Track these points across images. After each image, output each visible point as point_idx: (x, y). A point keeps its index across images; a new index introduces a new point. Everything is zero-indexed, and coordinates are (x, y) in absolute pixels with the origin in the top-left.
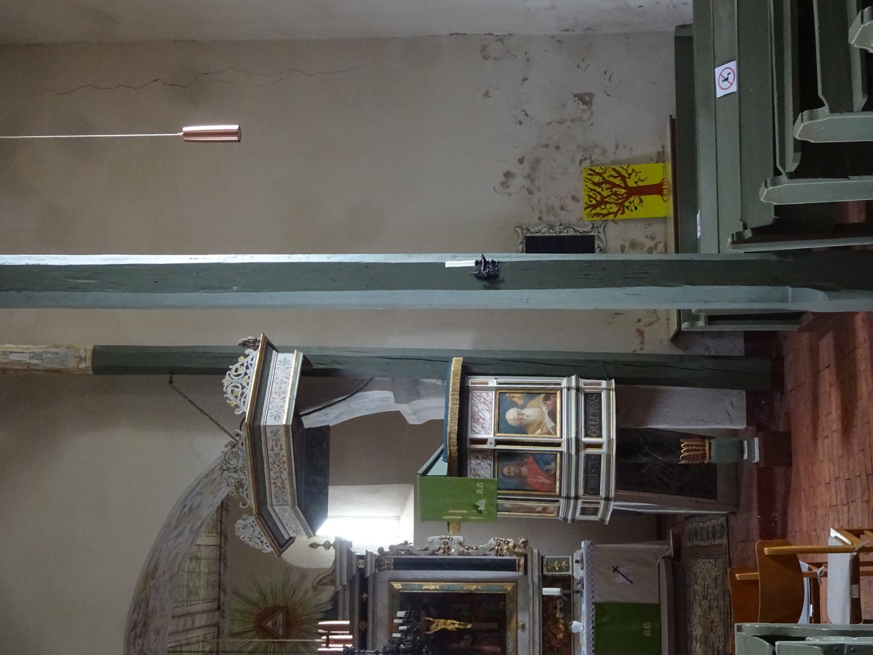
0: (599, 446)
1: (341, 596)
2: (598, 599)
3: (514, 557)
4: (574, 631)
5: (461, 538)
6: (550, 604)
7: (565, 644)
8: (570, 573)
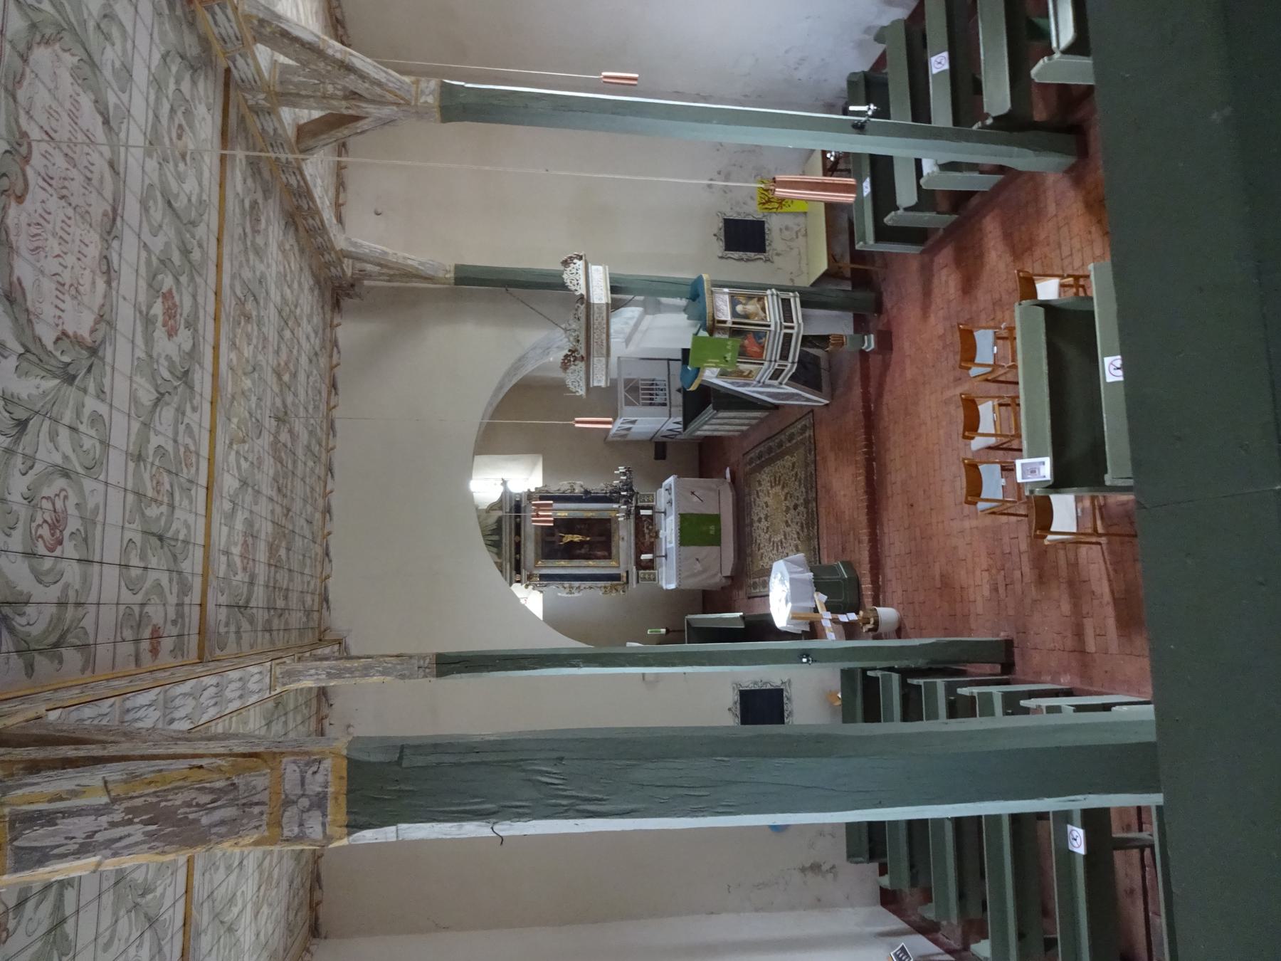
0: (792, 328)
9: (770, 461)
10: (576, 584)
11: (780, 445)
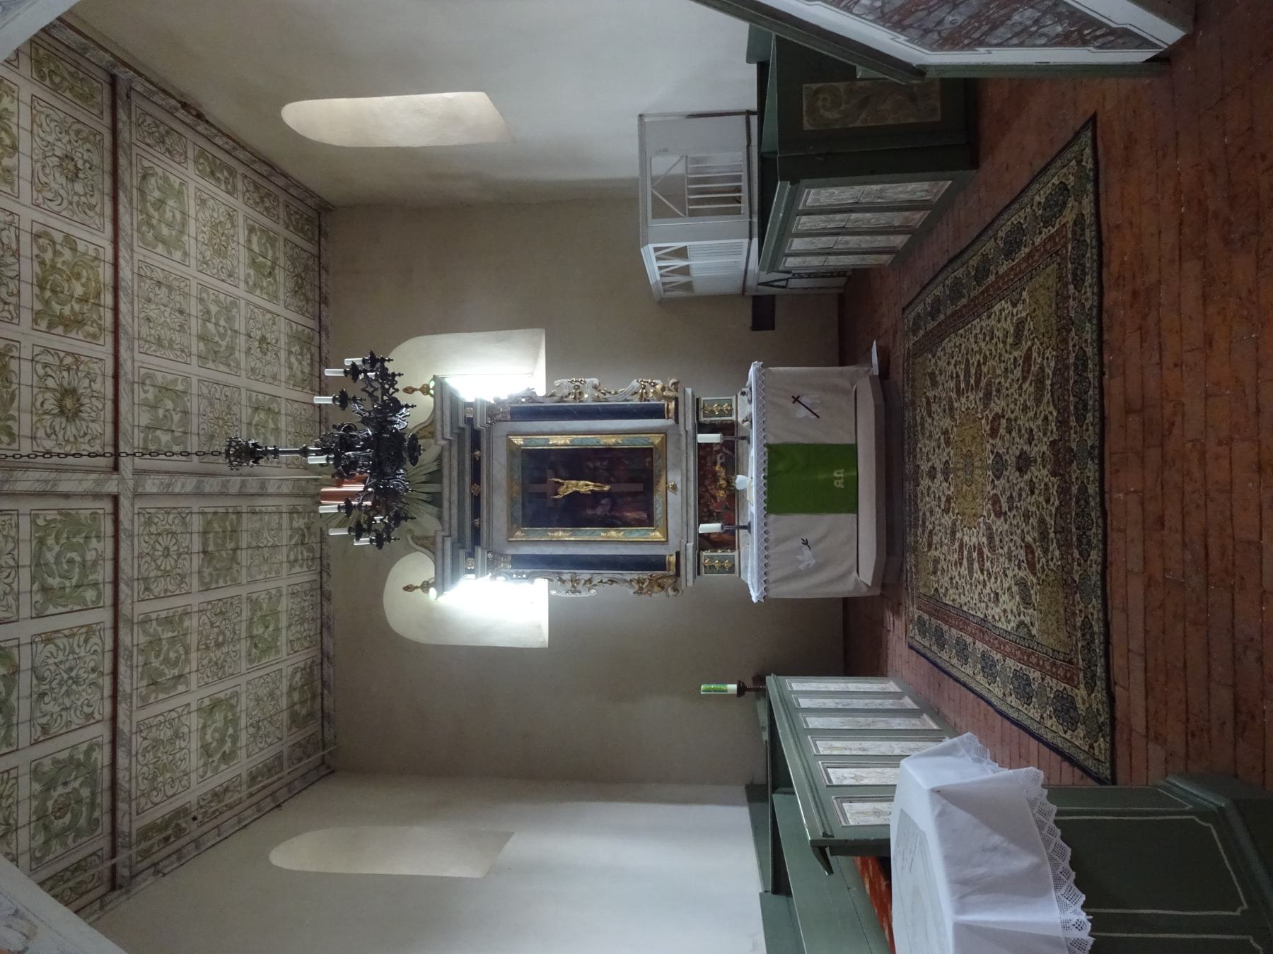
1: (446, 454)
2: (772, 440)
3: (663, 402)
4: (739, 487)
5: (596, 381)
6: (708, 459)
7: (726, 508)
8: (733, 418)
9: (959, 320)
10: (585, 574)
11: (982, 272)
